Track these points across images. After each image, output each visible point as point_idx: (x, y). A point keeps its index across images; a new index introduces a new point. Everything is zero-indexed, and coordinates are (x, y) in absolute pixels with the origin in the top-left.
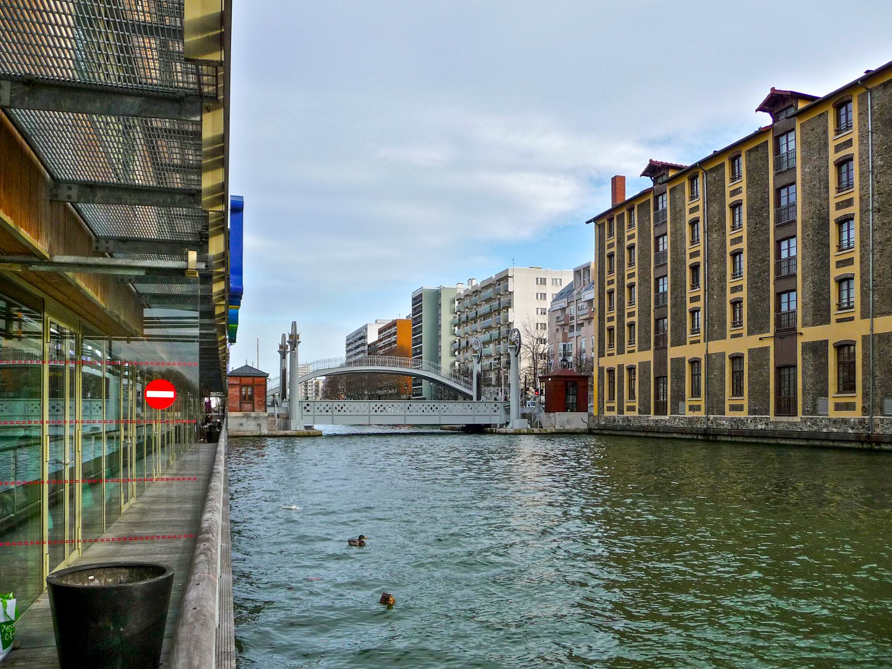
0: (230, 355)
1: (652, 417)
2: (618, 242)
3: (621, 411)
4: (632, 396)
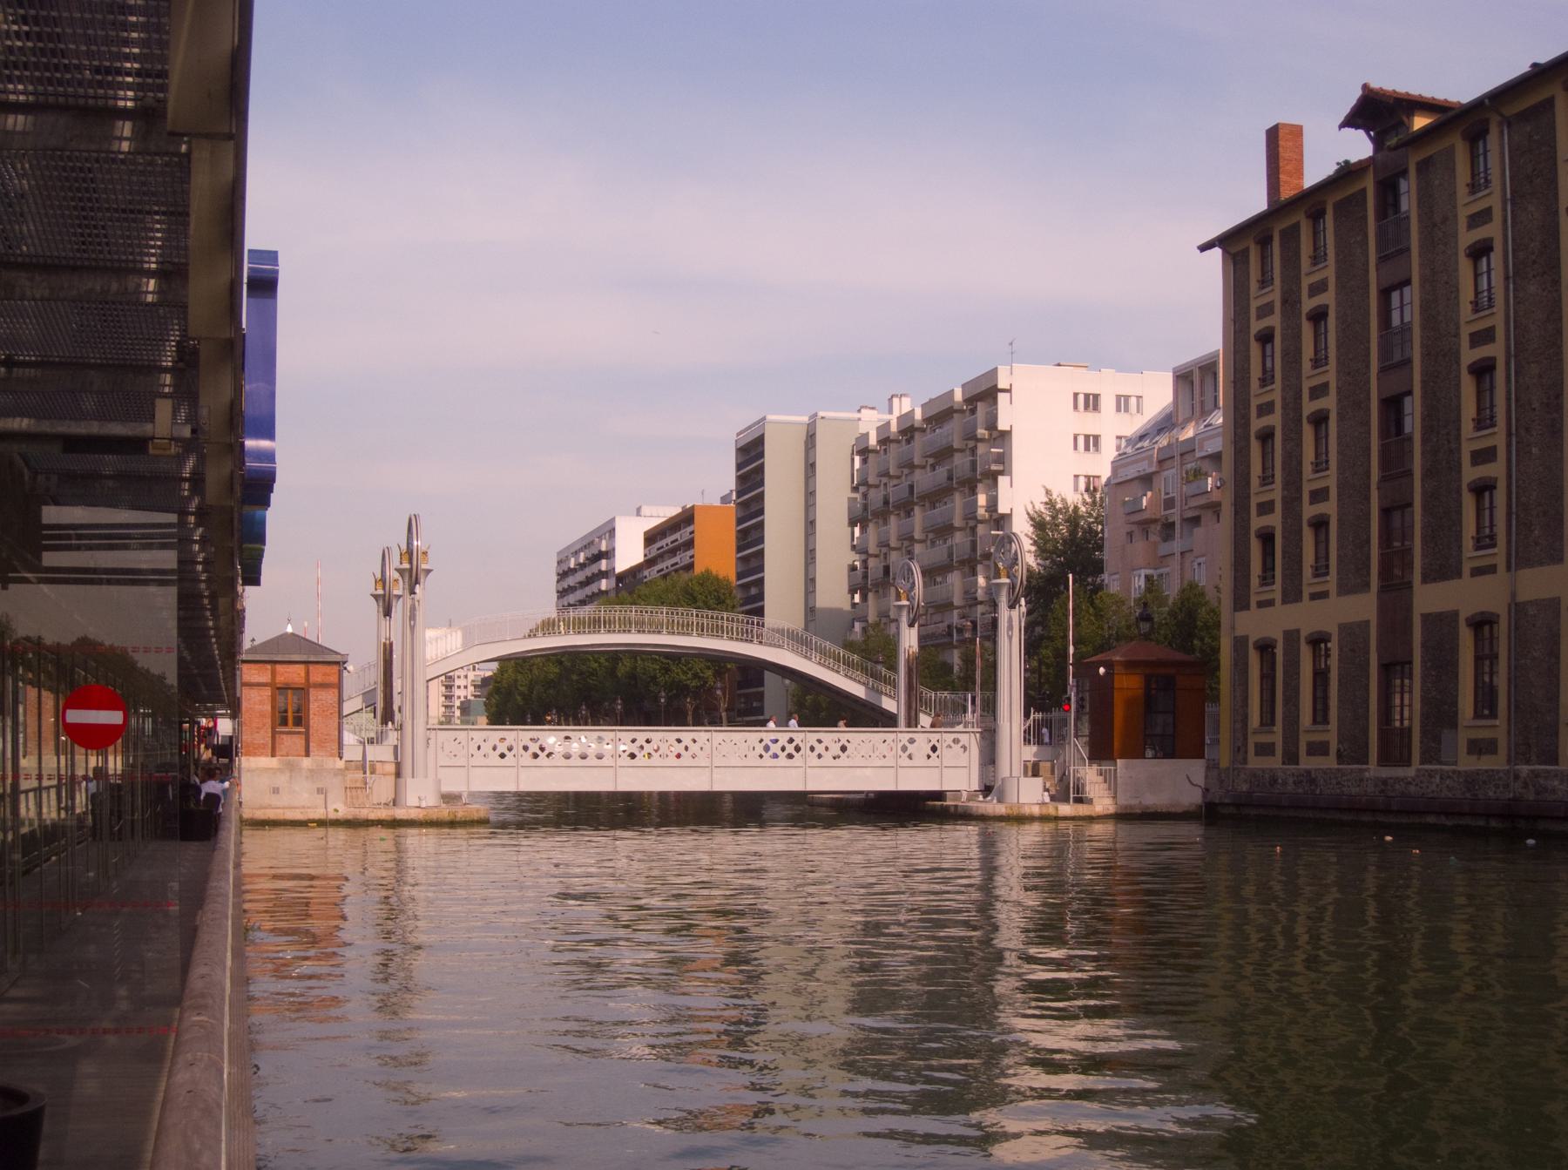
0: (248, 615)
2: (1284, 302)
3: (1291, 757)
4: (1320, 716)
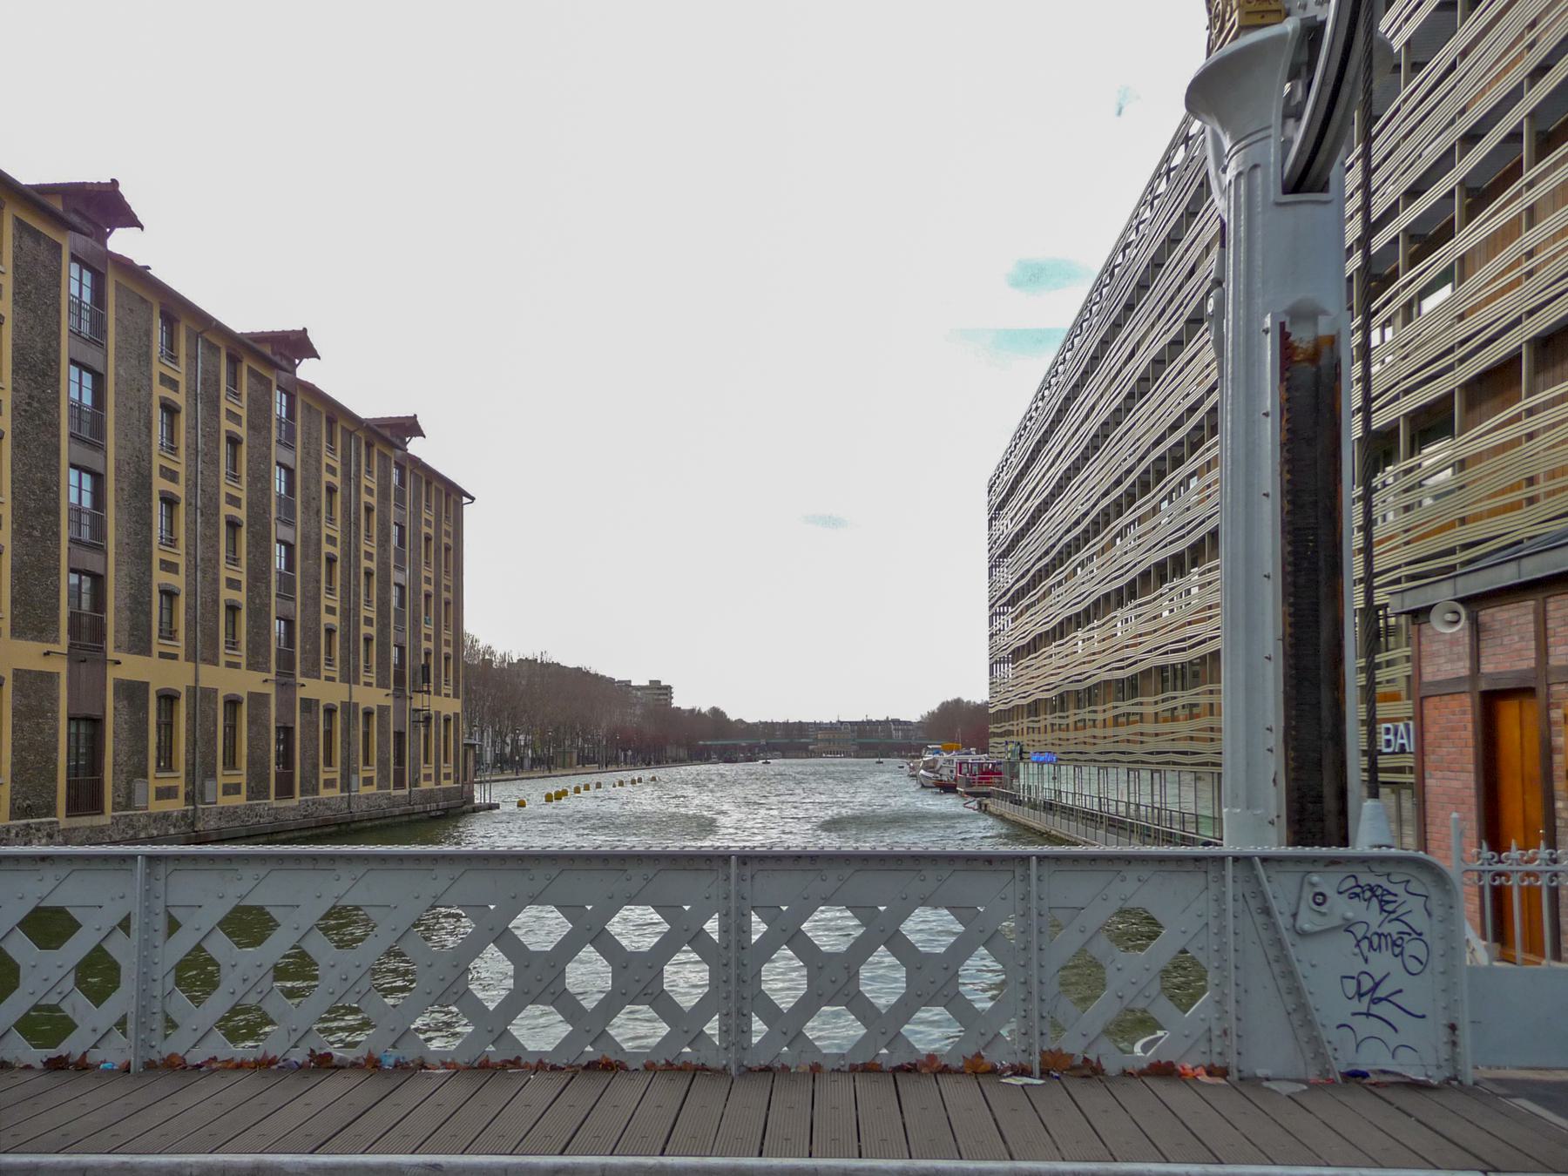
1: (272, 801)
